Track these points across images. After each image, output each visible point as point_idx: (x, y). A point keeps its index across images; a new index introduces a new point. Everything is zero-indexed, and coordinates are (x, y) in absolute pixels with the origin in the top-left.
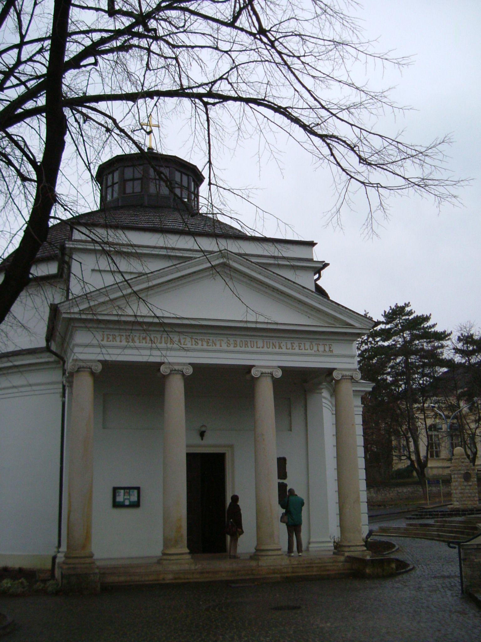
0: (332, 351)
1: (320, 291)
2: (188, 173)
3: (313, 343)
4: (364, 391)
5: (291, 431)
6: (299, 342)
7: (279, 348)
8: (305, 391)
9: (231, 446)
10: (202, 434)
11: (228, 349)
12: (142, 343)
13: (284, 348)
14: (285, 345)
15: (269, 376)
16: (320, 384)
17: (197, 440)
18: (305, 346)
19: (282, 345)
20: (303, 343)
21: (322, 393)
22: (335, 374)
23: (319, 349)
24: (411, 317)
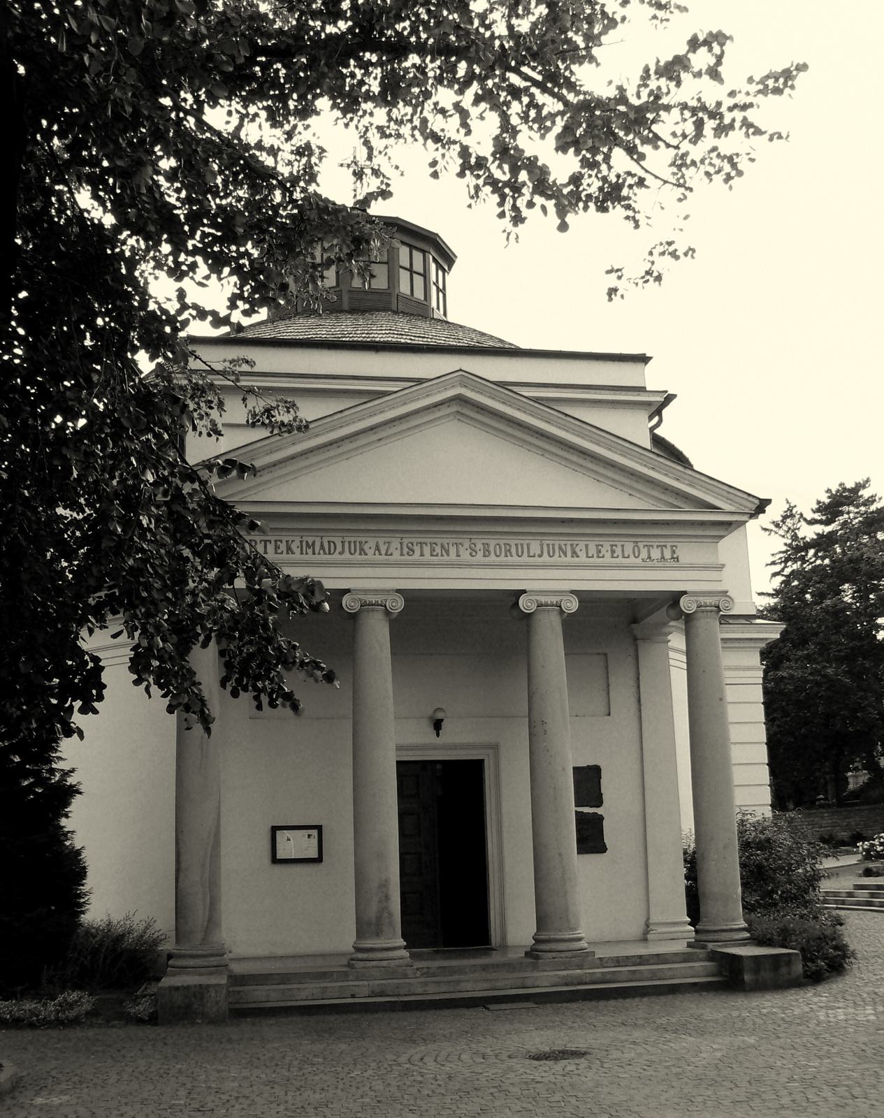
0: (677, 558)
1: (664, 448)
2: (426, 248)
3: (639, 544)
4: (766, 639)
5: (609, 715)
6: (598, 543)
7: (572, 557)
8: (635, 639)
9: (495, 748)
10: (437, 725)
11: (474, 560)
12: (307, 554)
13: (582, 554)
14: (584, 549)
15: (553, 610)
16: (665, 624)
17: (429, 737)
18: (623, 551)
19: (577, 550)
20: (619, 544)
21: (669, 641)
22: (684, 602)
23: (652, 555)
24: (873, 508)
